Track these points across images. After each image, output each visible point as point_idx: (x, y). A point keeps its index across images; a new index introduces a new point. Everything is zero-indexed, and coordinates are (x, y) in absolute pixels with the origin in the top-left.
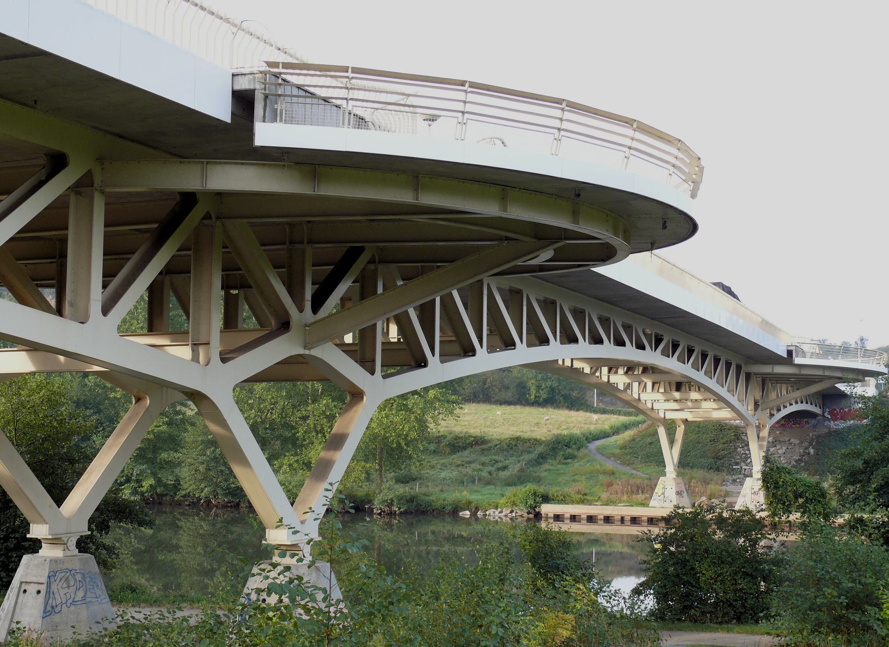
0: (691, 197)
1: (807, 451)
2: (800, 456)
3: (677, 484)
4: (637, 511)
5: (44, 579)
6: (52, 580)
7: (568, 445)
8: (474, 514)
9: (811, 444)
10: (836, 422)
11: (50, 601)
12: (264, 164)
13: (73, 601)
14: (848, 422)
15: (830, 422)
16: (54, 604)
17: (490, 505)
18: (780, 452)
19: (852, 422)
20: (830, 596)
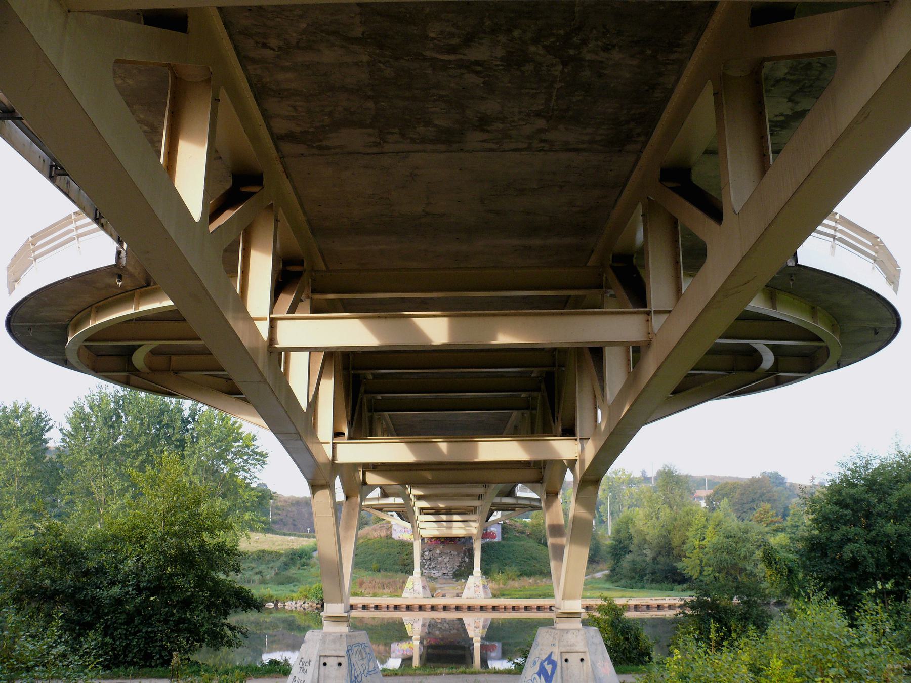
3: (422, 581)
5: (343, 653)
6: (351, 653)
7: (301, 557)
8: (276, 605)
9: (465, 555)
11: (353, 672)
12: (379, 317)
13: (368, 672)
16: (356, 675)
17: (287, 598)
18: (445, 560)
19: (488, 540)
20: (844, 645)
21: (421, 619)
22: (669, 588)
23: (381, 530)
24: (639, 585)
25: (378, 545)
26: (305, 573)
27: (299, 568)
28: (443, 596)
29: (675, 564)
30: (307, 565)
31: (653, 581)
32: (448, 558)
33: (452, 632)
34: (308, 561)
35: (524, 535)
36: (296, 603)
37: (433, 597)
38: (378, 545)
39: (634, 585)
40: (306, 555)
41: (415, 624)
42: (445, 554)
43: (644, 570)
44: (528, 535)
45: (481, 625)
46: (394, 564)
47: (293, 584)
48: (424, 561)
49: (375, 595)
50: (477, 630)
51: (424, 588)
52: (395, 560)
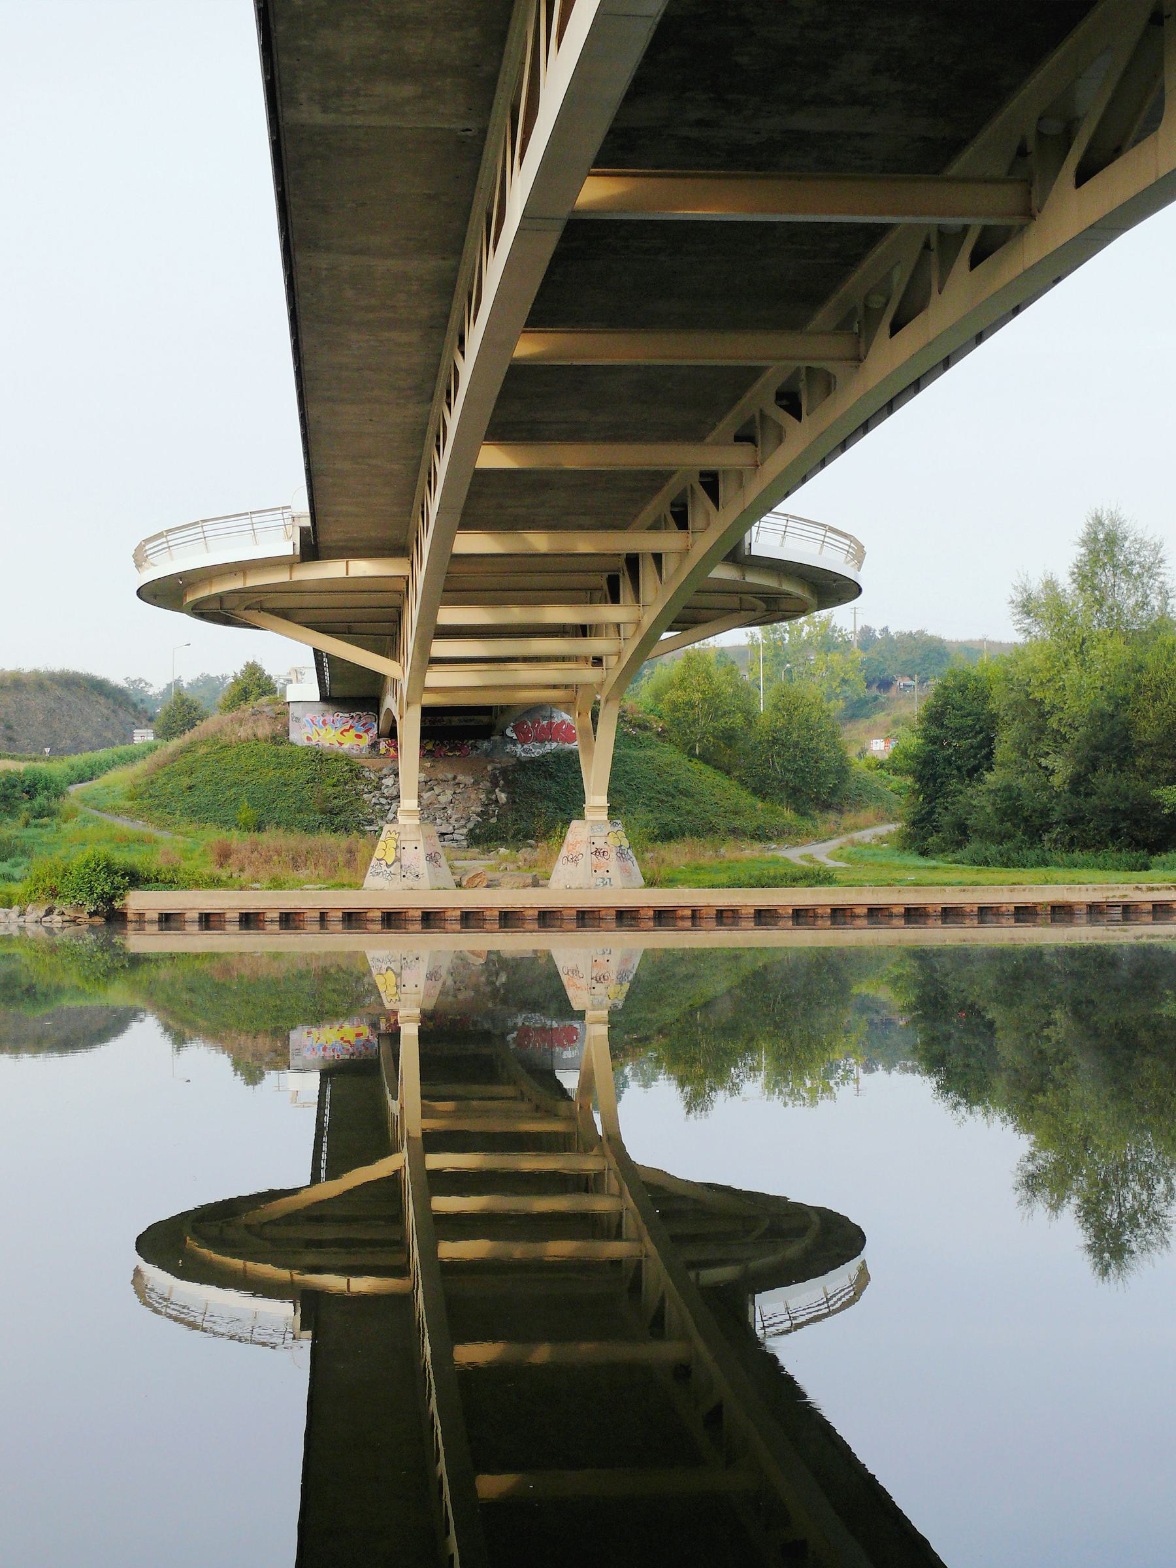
0: (860, 590)
1: (493, 797)
2: (483, 805)
4: (350, 900)
7: (31, 792)
9: (495, 784)
10: (525, 746)
14: (548, 746)
15: (515, 745)
19: (554, 745)
21: (425, 955)
22: (1127, 864)
23: (255, 721)
24: (1033, 855)
25: (252, 761)
26: (46, 836)
27: (27, 824)
28: (488, 886)
29: (1157, 792)
30: (52, 813)
31: (1071, 845)
32: (449, 792)
33: (461, 997)
34: (54, 805)
35: (648, 733)
36: (22, 914)
37: (459, 885)
38: (252, 761)
39: (1014, 855)
40: (46, 788)
41: (405, 973)
42: (439, 782)
43: (1044, 813)
44: (659, 734)
45: (613, 969)
46: (300, 811)
47: (11, 861)
48: (383, 801)
49: (277, 884)
50: (600, 988)
51: (431, 858)
52: (302, 801)
